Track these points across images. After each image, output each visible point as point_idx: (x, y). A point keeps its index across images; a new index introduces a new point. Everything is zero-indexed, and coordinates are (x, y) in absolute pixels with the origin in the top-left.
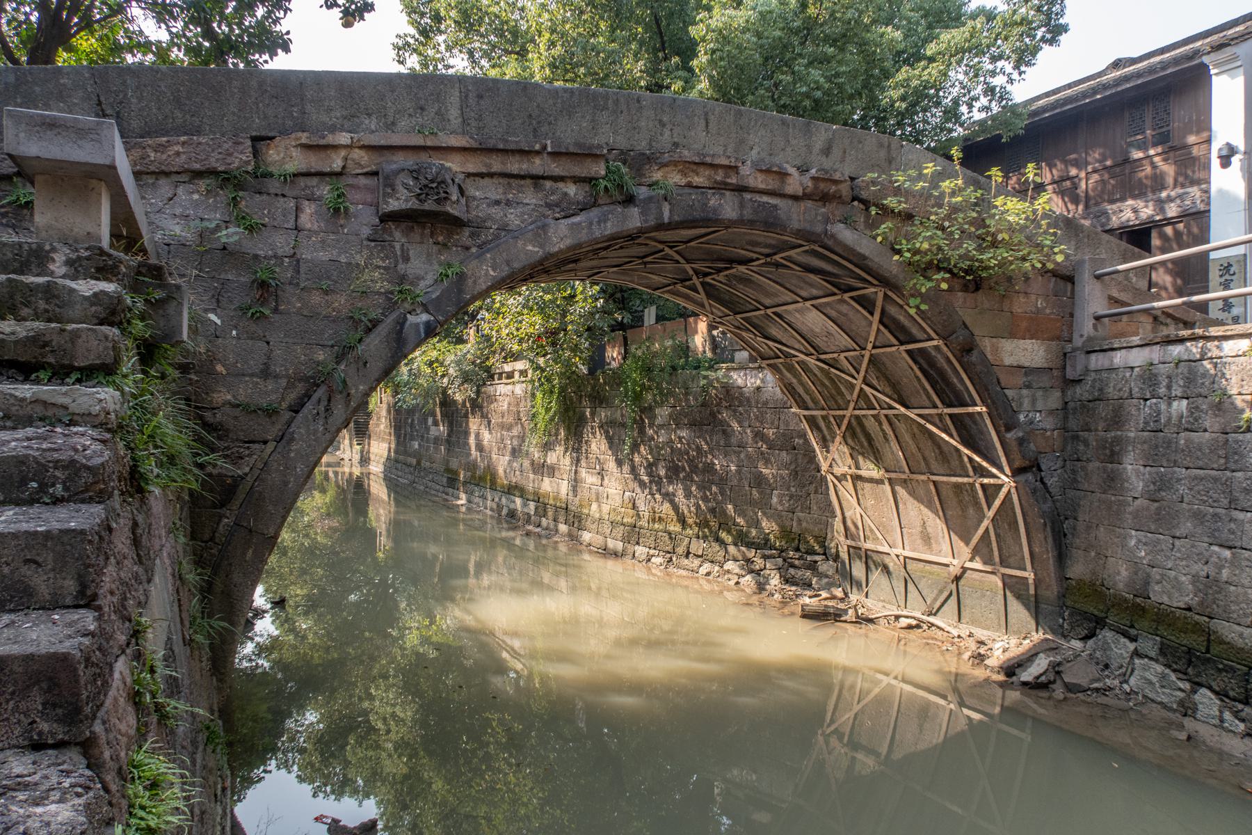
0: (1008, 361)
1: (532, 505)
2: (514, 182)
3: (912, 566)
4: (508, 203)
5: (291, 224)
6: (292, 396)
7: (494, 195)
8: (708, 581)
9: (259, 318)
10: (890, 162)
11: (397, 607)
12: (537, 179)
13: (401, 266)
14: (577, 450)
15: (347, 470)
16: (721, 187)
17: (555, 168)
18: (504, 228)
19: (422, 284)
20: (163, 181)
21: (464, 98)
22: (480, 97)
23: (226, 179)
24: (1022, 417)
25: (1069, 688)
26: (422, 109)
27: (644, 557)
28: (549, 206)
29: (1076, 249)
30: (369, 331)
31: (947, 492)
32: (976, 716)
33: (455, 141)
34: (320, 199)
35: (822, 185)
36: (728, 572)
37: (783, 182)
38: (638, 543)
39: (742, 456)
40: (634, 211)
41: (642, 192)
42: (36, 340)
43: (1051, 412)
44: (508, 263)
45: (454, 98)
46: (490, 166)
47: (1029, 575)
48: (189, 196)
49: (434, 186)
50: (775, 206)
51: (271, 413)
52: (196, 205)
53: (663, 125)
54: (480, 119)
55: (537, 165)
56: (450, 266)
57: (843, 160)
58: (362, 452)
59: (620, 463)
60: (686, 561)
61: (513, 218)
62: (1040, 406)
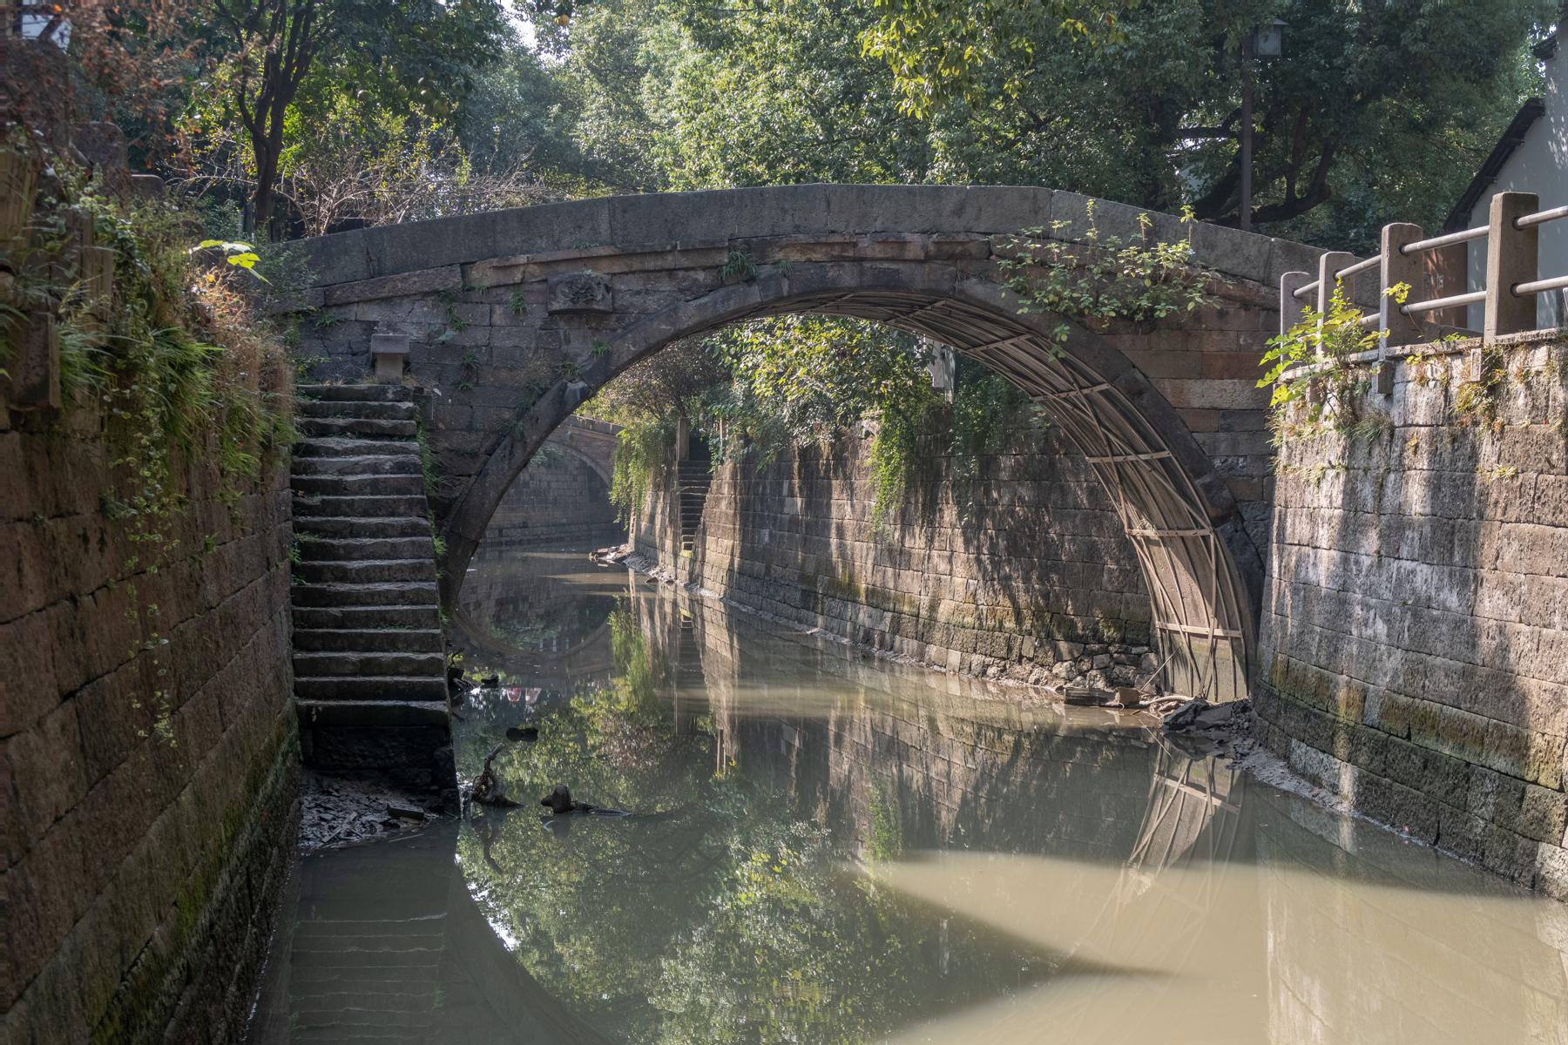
0: (1196, 403)
2: (652, 276)
4: (647, 292)
5: (487, 322)
6: (487, 444)
9: (465, 390)
12: (671, 272)
13: (564, 347)
14: (931, 523)
16: (838, 260)
17: (684, 262)
18: (644, 312)
19: (580, 360)
20: (406, 301)
21: (612, 215)
22: (624, 211)
23: (443, 296)
24: (1217, 463)
28: (681, 291)
30: (540, 396)
31: (1190, 544)
33: (603, 251)
35: (946, 248)
40: (755, 289)
42: (395, 427)
48: (422, 309)
49: (584, 291)
51: (474, 455)
53: (784, 211)
55: (670, 261)
57: (978, 218)
58: (693, 561)
59: (967, 542)
60: (1018, 668)
61: (651, 303)
62: (1243, 449)
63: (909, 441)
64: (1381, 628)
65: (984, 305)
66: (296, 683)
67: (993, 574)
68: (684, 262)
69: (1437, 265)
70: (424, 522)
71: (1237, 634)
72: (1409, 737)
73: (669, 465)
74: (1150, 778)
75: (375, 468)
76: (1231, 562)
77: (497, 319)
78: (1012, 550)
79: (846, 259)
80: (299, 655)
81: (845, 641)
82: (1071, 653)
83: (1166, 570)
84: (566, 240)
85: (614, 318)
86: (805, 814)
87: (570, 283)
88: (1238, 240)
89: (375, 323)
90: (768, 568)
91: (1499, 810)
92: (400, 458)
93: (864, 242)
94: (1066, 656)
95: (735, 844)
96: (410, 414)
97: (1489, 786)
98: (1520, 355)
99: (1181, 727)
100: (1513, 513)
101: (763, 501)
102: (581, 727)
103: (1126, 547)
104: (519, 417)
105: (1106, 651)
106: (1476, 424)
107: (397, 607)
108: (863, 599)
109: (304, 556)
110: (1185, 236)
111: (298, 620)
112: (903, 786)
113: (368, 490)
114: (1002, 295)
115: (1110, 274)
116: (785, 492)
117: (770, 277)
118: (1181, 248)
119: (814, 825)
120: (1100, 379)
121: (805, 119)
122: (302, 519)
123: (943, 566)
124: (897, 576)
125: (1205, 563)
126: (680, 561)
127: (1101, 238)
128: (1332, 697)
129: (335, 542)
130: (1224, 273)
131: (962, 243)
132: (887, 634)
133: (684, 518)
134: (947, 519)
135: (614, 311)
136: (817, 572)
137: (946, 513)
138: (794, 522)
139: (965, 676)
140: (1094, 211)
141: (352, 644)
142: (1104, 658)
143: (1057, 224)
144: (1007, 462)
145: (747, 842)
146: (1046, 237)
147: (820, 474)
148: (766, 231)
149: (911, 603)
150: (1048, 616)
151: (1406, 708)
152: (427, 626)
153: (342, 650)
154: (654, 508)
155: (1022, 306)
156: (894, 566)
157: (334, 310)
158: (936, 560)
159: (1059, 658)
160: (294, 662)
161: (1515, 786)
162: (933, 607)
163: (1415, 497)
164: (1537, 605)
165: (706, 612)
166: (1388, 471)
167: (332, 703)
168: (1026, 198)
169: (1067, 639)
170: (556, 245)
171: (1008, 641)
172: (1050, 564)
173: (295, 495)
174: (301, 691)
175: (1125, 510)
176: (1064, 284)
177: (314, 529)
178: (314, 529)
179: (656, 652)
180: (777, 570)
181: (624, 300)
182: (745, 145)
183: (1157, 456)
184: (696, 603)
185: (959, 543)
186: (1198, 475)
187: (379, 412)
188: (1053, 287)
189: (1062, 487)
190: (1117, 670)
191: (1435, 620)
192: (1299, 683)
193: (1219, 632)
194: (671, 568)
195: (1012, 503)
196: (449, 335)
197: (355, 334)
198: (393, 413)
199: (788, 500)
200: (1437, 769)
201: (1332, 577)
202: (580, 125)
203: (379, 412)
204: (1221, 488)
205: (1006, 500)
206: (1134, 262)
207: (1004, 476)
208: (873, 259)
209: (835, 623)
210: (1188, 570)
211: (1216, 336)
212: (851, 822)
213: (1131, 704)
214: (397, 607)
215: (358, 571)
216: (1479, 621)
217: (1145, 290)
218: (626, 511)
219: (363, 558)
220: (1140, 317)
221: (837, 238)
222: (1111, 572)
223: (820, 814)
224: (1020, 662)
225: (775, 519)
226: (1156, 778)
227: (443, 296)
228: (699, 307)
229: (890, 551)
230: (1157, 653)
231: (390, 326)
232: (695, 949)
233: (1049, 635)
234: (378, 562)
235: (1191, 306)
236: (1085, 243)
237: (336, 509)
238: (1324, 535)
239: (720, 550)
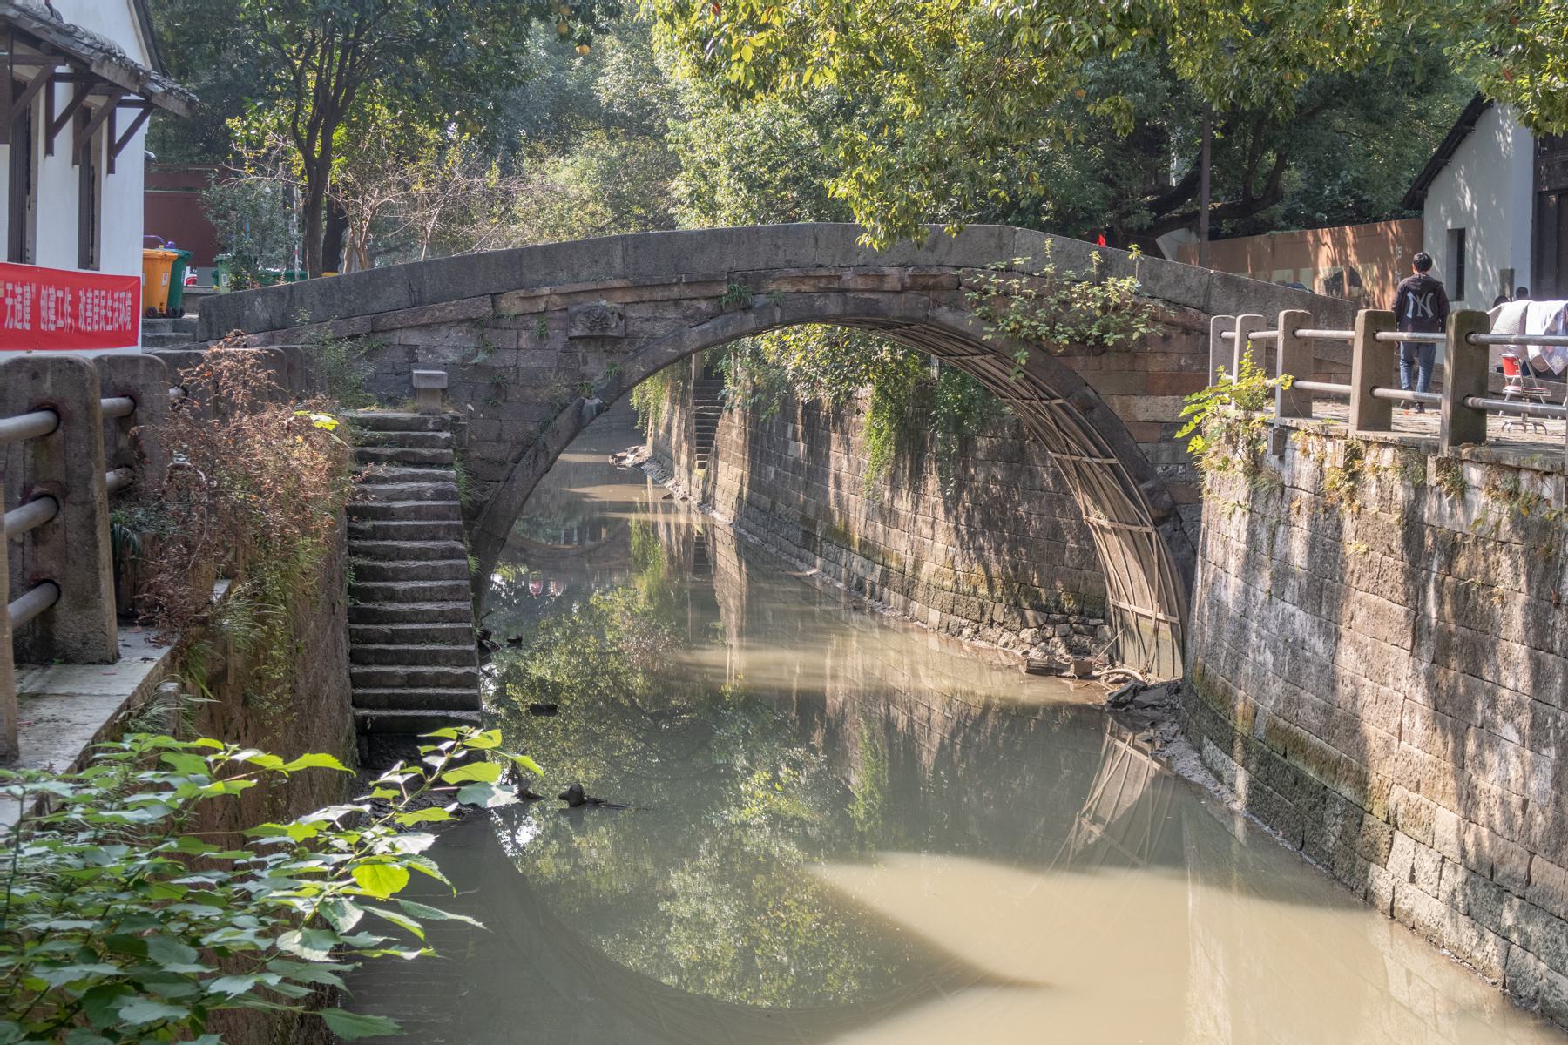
0: (1141, 417)
4: (656, 319)
6: (514, 454)
7: (645, 315)
8: (1005, 653)
9: (495, 405)
12: (676, 302)
15: (683, 520)
16: (825, 291)
17: (689, 293)
18: (652, 337)
21: (625, 250)
22: (636, 247)
23: (476, 323)
24: (1159, 470)
28: (686, 318)
33: (616, 283)
35: (920, 280)
42: (435, 456)
48: (457, 335)
49: (599, 318)
50: (877, 301)
51: (502, 463)
52: (460, 339)
53: (777, 247)
54: (637, 262)
55: (675, 292)
57: (949, 253)
58: (706, 481)
59: (947, 511)
60: (989, 631)
61: (659, 329)
63: (898, 415)
64: (1269, 657)
65: (954, 330)
66: (354, 696)
67: (968, 541)
68: (689, 293)
69: (1396, 236)
70: (461, 547)
71: (1175, 620)
72: (1285, 755)
73: (686, 382)
74: (1103, 737)
75: (418, 496)
77: (523, 343)
78: (986, 523)
79: (831, 290)
80: (356, 669)
81: (840, 585)
82: (1036, 620)
83: (1117, 555)
84: (584, 274)
85: (626, 342)
86: (803, 737)
87: (588, 314)
89: (416, 347)
90: (773, 504)
91: (1344, 831)
92: (439, 485)
93: (848, 275)
94: (1032, 623)
95: (741, 761)
96: (447, 444)
97: (1339, 810)
98: (1373, 451)
99: (1122, 705)
100: (1364, 584)
101: (770, 438)
102: (598, 622)
103: (1084, 532)
104: (542, 430)
105: (1067, 622)
106: (1341, 500)
107: (438, 626)
108: (856, 548)
109: (358, 578)
110: (1132, 273)
111: (355, 637)
112: (889, 725)
114: (969, 322)
115: (1066, 304)
116: (790, 435)
117: (764, 306)
118: (1129, 283)
119: (812, 749)
121: (802, 127)
122: (356, 543)
123: (926, 531)
124: (887, 534)
125: (1149, 556)
126: (694, 479)
127: (1058, 273)
128: (1233, 707)
129: (384, 564)
130: (1167, 301)
131: (934, 276)
132: (872, 592)
133: (698, 437)
134: (930, 487)
135: (627, 336)
136: (817, 515)
137: (930, 482)
138: (797, 464)
139: (944, 635)
140: (1052, 248)
141: (400, 658)
142: (1066, 627)
144: (982, 443)
145: (751, 760)
146: (1010, 270)
147: (821, 426)
148: (762, 265)
149: (898, 560)
150: (1016, 586)
151: (1284, 731)
152: (464, 643)
153: (391, 664)
154: (670, 420)
155: (987, 333)
156: (884, 522)
158: (920, 524)
160: (352, 676)
161: (1357, 814)
162: (917, 566)
163: (1298, 550)
164: (1377, 665)
165: (718, 533)
166: (1279, 522)
167: (384, 713)
168: (992, 235)
169: (1034, 608)
170: (576, 278)
171: (981, 606)
172: (1019, 539)
173: (350, 520)
174: (358, 702)
175: (1082, 499)
176: (1024, 314)
177: (368, 553)
178: (368, 553)
179: (672, 559)
180: (781, 507)
181: (635, 326)
182: (749, 150)
183: (1106, 461)
184: (710, 528)
185: (941, 511)
186: (1142, 481)
187: (421, 442)
189: (1030, 471)
190: (1076, 638)
191: (1307, 661)
192: (1210, 687)
193: (1161, 616)
194: (685, 482)
195: (986, 481)
196: (481, 357)
197: (400, 356)
198: (432, 442)
199: (792, 443)
200: (1304, 787)
201: (1236, 602)
202: (601, 80)
203: (421, 442)
204: (1162, 492)
205: (982, 476)
206: (1087, 297)
207: (980, 455)
208: (855, 290)
209: (832, 567)
211: (1159, 358)
212: (845, 750)
213: (1084, 674)
214: (438, 626)
215: (404, 591)
216: (1338, 669)
217: (1096, 319)
218: (645, 416)
219: (408, 579)
220: (1091, 342)
221: (824, 272)
222: (1072, 550)
223: (818, 738)
225: (780, 458)
226: (1107, 737)
227: (476, 323)
228: (701, 333)
229: (881, 507)
231: (429, 349)
232: (701, 862)
233: (1017, 604)
234: (421, 584)
235: (1135, 336)
236: (1044, 276)
237: (385, 534)
238: (1234, 564)
239: (731, 476)
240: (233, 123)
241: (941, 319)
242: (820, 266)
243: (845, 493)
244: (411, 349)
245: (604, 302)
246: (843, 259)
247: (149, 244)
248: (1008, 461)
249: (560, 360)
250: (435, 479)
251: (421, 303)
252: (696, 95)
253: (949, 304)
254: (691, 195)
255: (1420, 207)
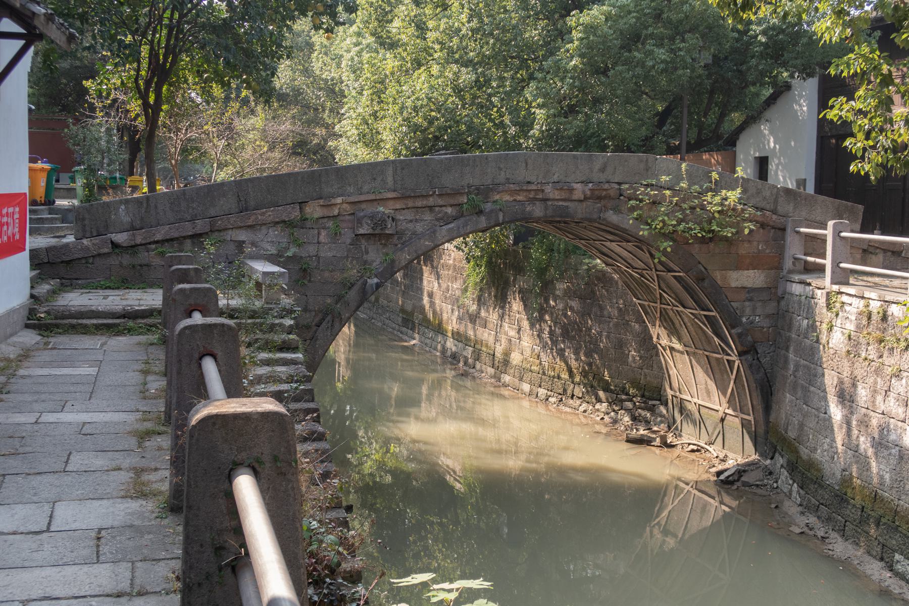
0: (733, 285)
1: (470, 349)
2: (420, 210)
3: (703, 410)
4: (416, 221)
5: (316, 241)
6: (317, 320)
7: (409, 218)
8: (585, 417)
10: (647, 170)
11: (356, 437)
12: (431, 208)
13: (365, 256)
14: (503, 308)
16: (533, 200)
18: (414, 233)
19: (375, 264)
20: (263, 227)
22: (403, 169)
23: (288, 224)
24: (744, 320)
25: (746, 484)
26: (375, 179)
27: (543, 397)
28: (438, 220)
29: (794, 208)
30: (350, 288)
31: (714, 363)
32: (727, 509)
34: (328, 228)
35: (597, 192)
36: (598, 410)
37: (572, 193)
38: (540, 386)
39: (611, 325)
40: (483, 218)
41: (488, 207)
43: (768, 316)
44: (416, 251)
45: (390, 172)
46: (407, 204)
47: (751, 418)
49: (380, 222)
50: (567, 207)
52: (276, 236)
53: (500, 169)
55: (431, 201)
56: (387, 254)
57: (614, 173)
59: (532, 326)
60: (571, 402)
62: (759, 311)
65: (617, 227)
76: (751, 379)
77: (322, 238)
79: (537, 199)
82: (607, 399)
84: (366, 188)
87: (372, 217)
88: (760, 187)
89: (244, 242)
93: (548, 189)
105: (631, 400)
108: (450, 334)
113: (192, 273)
117: (492, 211)
120: (677, 268)
143: (664, 178)
148: (489, 182)
157: (216, 233)
159: (599, 400)
168: (642, 161)
181: (403, 226)
183: (702, 312)
186: (733, 327)
188: (664, 218)
210: (706, 372)
211: (746, 245)
221: (534, 187)
224: (572, 398)
227: (288, 224)
230: (666, 405)
231: (253, 244)
240: (87, 84)
241: (609, 219)
242: (529, 182)
243: (437, 302)
244: (240, 245)
245: (381, 209)
246: (544, 178)
247: (32, 160)
248: (582, 298)
249: (349, 250)
250: (286, 362)
251: (247, 210)
252: (369, 75)
253: (613, 209)
254: (359, 135)
255: (734, 145)
